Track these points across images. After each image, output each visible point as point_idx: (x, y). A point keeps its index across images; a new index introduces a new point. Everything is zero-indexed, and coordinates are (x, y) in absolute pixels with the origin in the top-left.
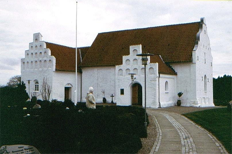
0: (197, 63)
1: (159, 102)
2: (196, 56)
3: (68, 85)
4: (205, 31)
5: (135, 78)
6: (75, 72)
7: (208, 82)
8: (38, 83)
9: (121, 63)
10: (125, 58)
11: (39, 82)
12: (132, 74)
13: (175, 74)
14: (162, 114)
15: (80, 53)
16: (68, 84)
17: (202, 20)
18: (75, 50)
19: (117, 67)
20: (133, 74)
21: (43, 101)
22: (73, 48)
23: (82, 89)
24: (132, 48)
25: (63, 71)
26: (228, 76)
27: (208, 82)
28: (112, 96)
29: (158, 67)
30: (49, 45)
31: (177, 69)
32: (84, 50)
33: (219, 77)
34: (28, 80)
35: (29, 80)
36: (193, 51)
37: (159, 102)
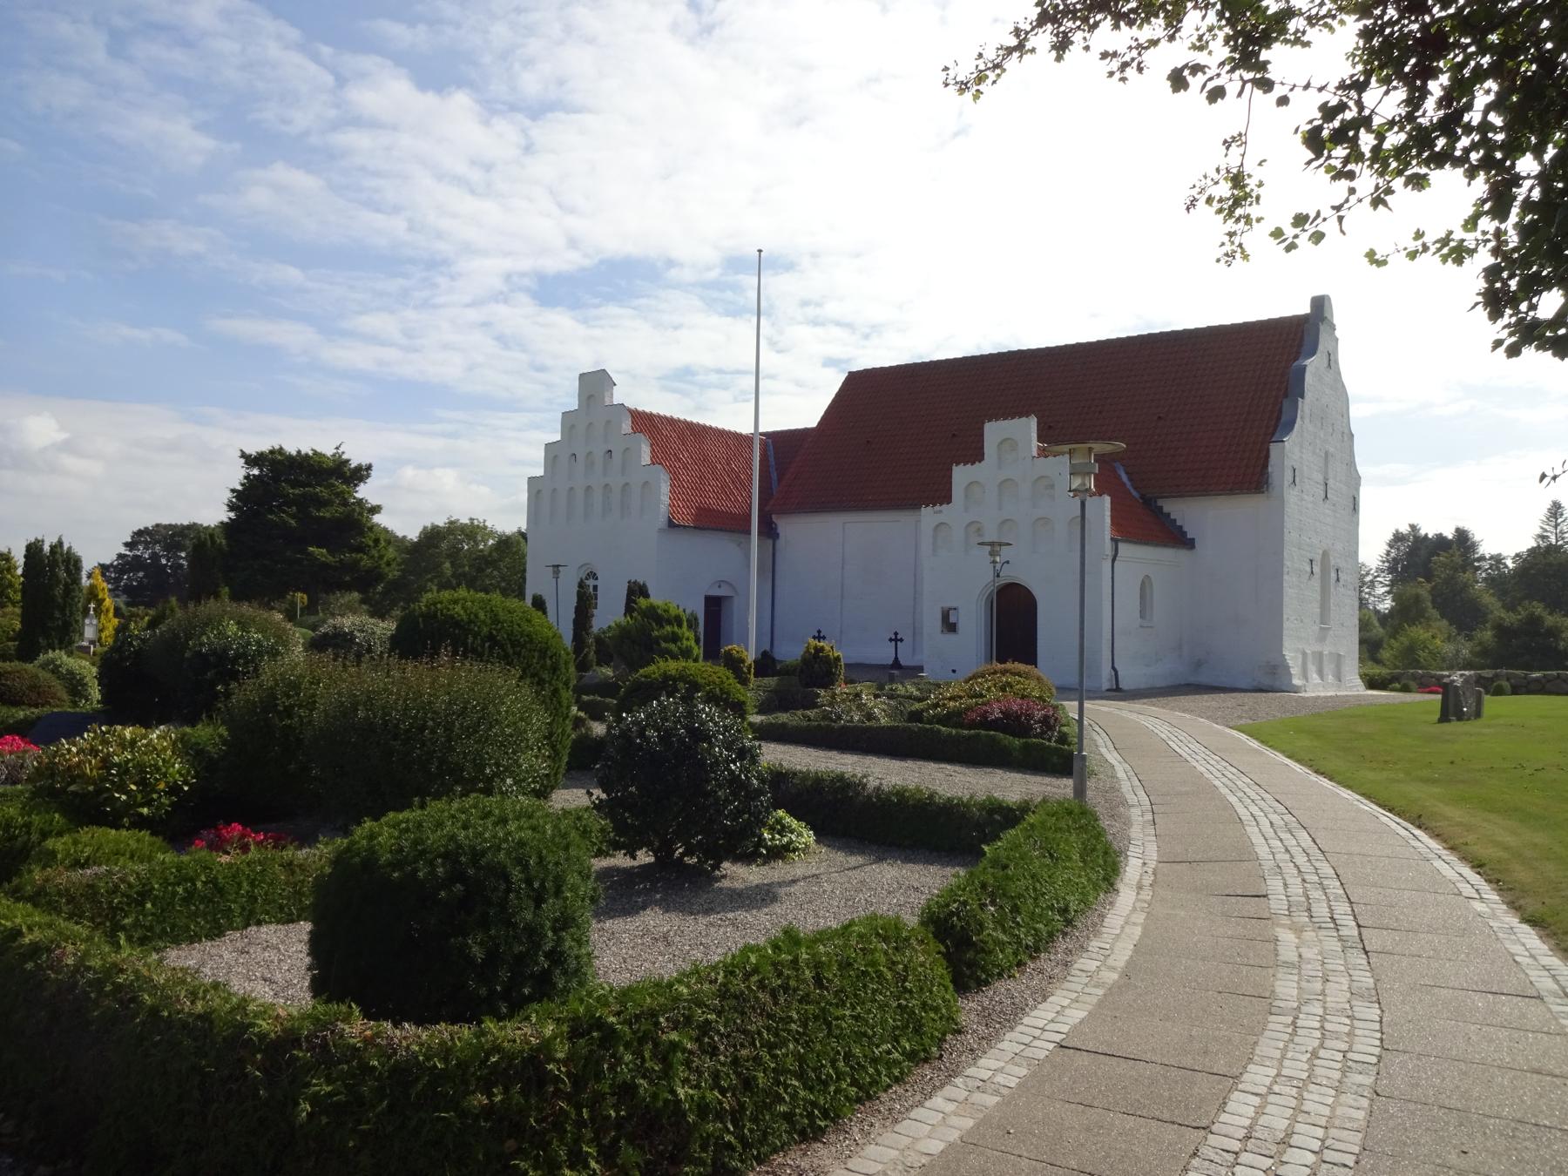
0: (1291, 497)
1: (1113, 668)
2: (1288, 463)
3: (720, 587)
4: (1329, 354)
5: (1008, 562)
6: (748, 532)
7: (1338, 580)
8: (597, 579)
9: (946, 498)
10: (961, 475)
11: (599, 575)
12: (992, 544)
13: (1177, 538)
14: (1134, 716)
15: (772, 459)
16: (720, 584)
17: (1320, 304)
18: (751, 447)
19: (926, 511)
20: (1001, 544)
21: (18, 735)
22: (741, 435)
23: (776, 601)
24: (994, 432)
25: (713, 529)
26: (232, 507)
27: (1338, 580)
28: (896, 640)
29: (1108, 513)
30: (645, 423)
31: (1186, 512)
32: (783, 445)
33: (360, 474)
34: (554, 566)
35: (558, 566)
36: (1236, 1095)
37: (1113, 668)
